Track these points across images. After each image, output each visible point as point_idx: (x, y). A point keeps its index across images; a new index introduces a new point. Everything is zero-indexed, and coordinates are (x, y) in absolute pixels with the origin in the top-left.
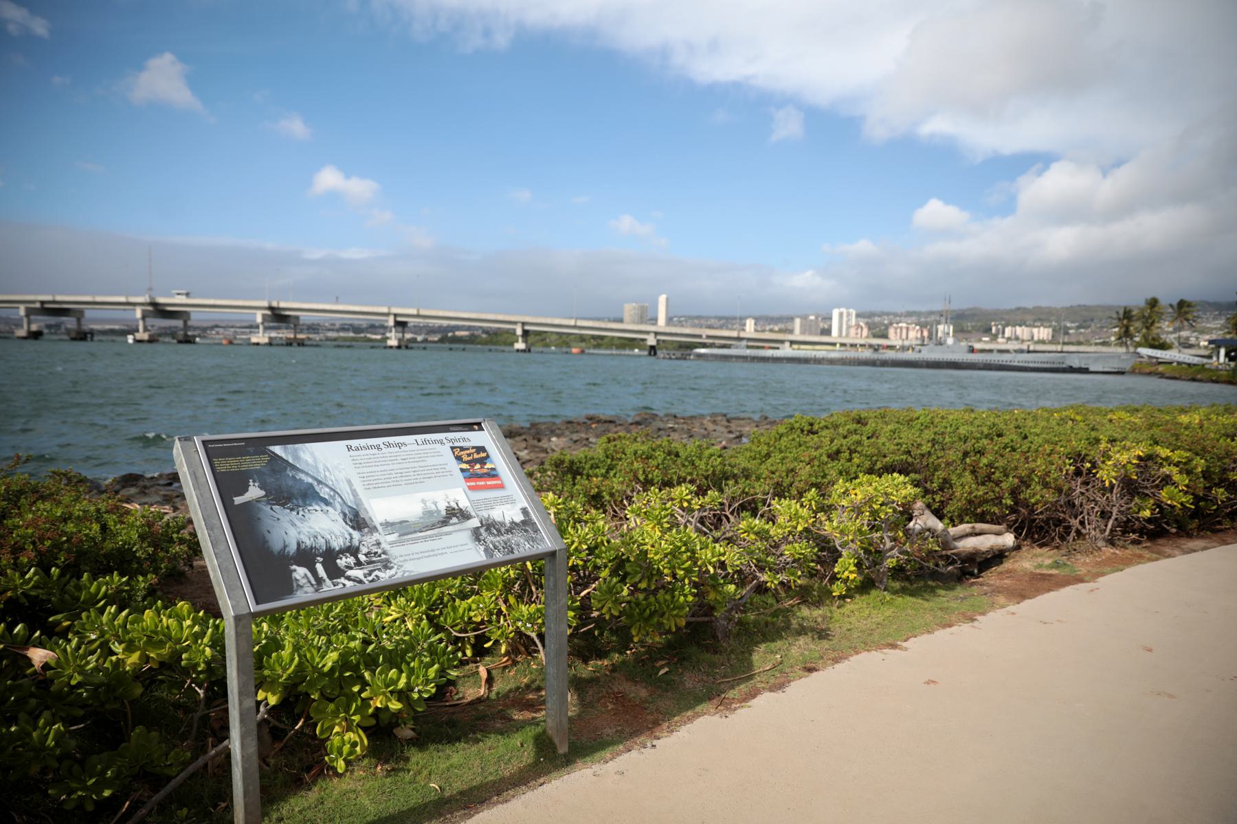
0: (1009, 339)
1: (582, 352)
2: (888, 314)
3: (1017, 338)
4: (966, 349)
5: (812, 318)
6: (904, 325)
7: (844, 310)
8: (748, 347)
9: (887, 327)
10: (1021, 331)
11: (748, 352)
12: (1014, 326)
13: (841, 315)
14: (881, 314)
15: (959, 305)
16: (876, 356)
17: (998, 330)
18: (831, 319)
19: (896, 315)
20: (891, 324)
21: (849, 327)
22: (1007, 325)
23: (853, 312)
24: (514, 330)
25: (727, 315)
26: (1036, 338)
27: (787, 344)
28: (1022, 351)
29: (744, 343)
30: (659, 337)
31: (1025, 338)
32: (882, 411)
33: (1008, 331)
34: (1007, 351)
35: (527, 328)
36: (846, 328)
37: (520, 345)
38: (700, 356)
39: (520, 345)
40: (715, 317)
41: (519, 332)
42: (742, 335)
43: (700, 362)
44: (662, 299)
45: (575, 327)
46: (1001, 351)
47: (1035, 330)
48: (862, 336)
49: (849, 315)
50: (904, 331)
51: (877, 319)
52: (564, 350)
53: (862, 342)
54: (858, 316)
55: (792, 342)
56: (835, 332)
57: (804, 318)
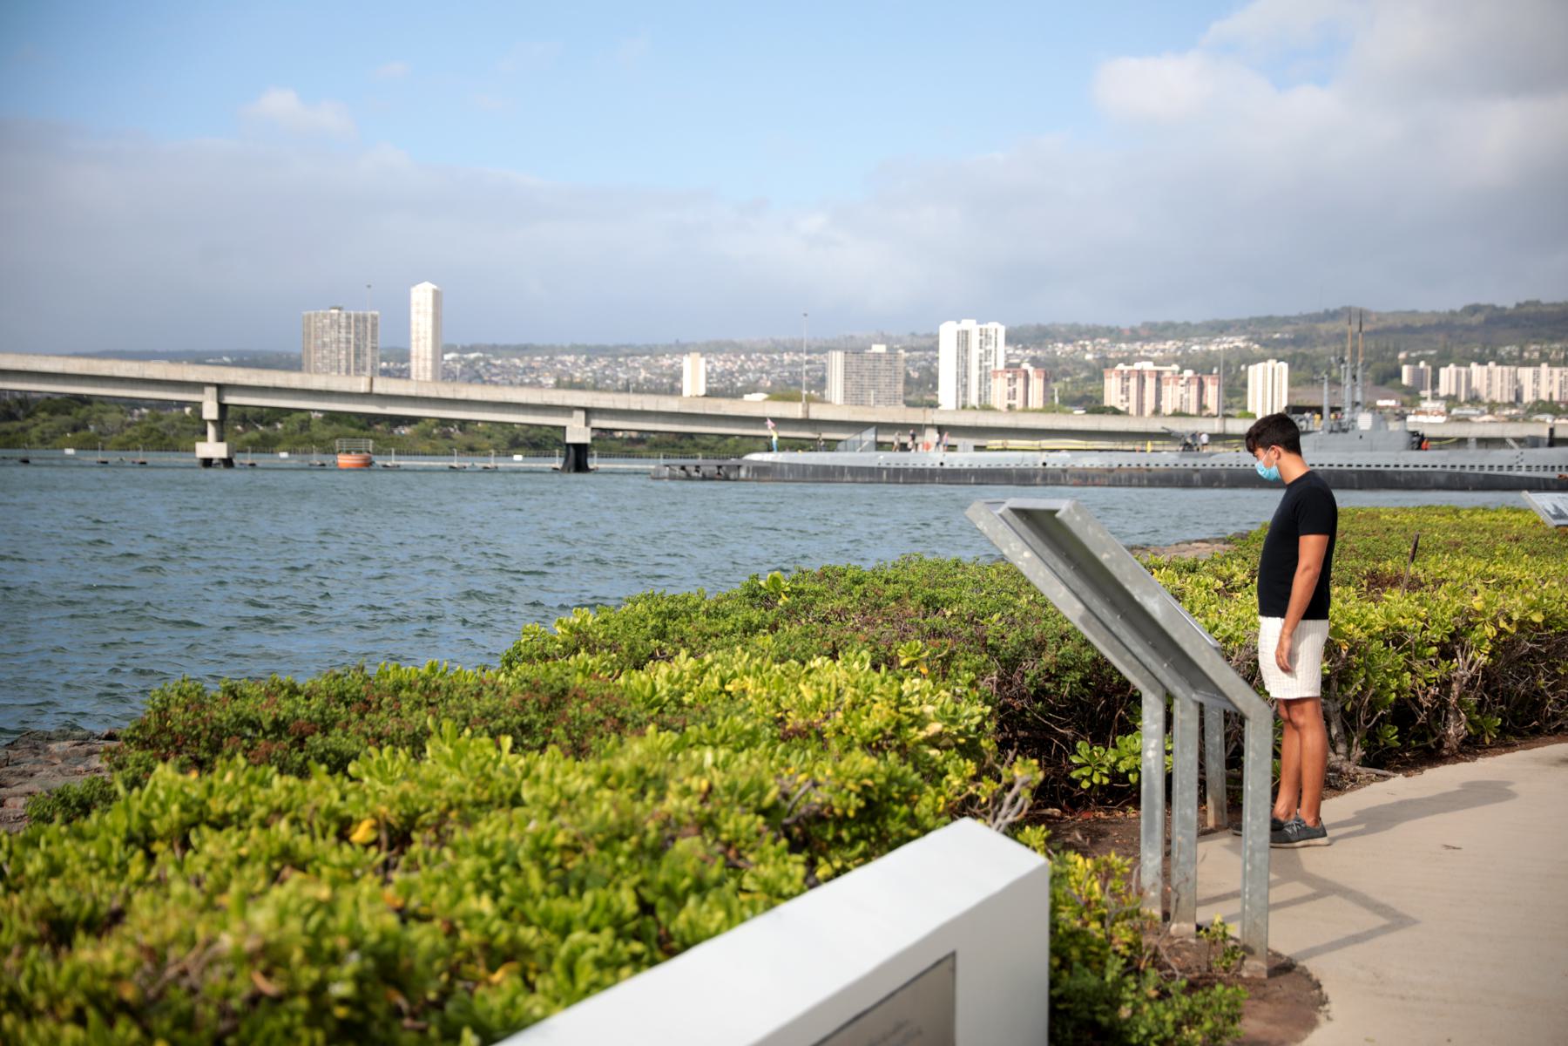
0: (1452, 400)
1: (368, 464)
2: (1093, 333)
3: (1474, 400)
4: (1403, 440)
5: (880, 348)
6: (1148, 366)
7: (970, 325)
8: (880, 446)
9: (1097, 373)
10: (1488, 379)
11: (883, 459)
12: (1464, 361)
13: (963, 339)
14: (1073, 334)
15: (1295, 301)
16: (1190, 462)
17: (1418, 376)
18: (935, 347)
19: (1115, 334)
20: (1105, 364)
21: (985, 378)
22: (1443, 360)
23: (998, 330)
24: (197, 407)
25: (610, 342)
26: (1528, 397)
27: (932, 436)
28: (1534, 442)
29: (869, 436)
30: (597, 423)
31: (1497, 396)
32: (893, 724)
33: (1448, 375)
34: (1500, 442)
35: (230, 399)
36: (978, 372)
37: (212, 448)
38: (762, 471)
39: (212, 448)
40: (574, 349)
41: (210, 411)
42: (817, 412)
43: (768, 488)
44: (422, 297)
45: (368, 396)
46: (1484, 442)
47: (1526, 374)
48: (1016, 397)
49: (985, 337)
50: (1150, 384)
51: (1061, 349)
52: (316, 459)
53: (1216, 426)
54: (1011, 339)
55: (941, 429)
56: (947, 394)
57: (856, 351)
